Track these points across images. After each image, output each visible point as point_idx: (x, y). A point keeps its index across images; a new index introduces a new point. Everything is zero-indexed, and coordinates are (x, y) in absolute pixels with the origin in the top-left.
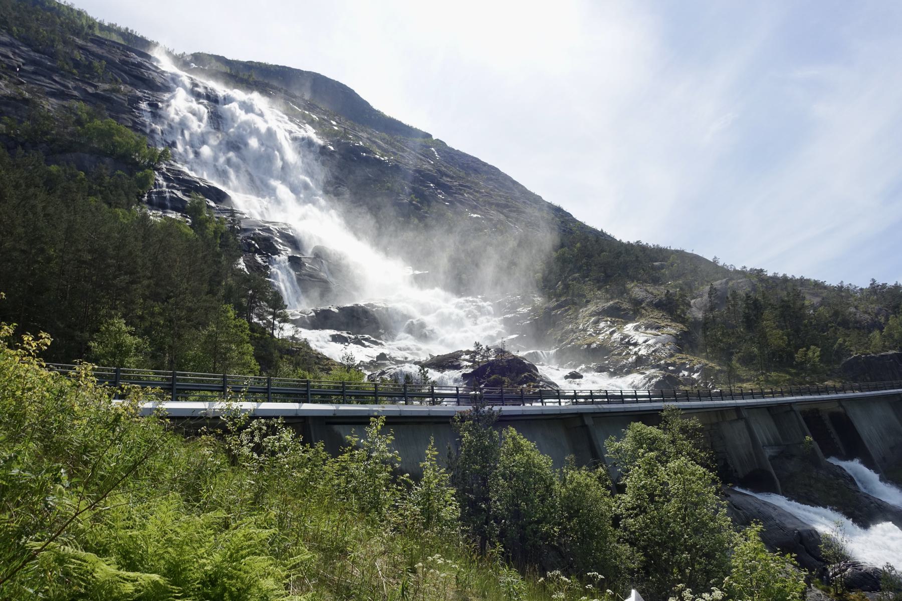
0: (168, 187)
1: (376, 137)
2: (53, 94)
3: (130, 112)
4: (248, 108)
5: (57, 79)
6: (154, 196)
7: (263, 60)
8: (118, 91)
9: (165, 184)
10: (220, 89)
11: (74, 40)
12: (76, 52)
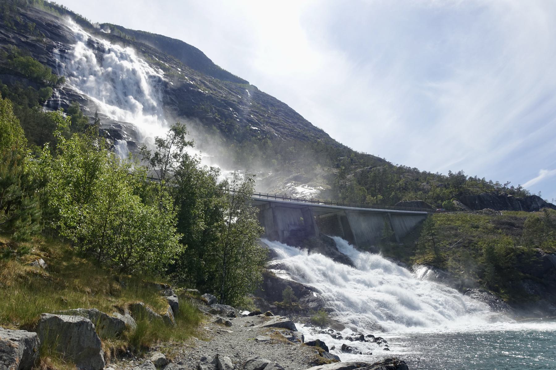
0: (61, 98)
1: (206, 80)
3: (47, 54)
5: (2, 32)
6: (51, 102)
7: (147, 30)
8: (41, 41)
9: (60, 96)
11: (18, 10)
12: (17, 17)
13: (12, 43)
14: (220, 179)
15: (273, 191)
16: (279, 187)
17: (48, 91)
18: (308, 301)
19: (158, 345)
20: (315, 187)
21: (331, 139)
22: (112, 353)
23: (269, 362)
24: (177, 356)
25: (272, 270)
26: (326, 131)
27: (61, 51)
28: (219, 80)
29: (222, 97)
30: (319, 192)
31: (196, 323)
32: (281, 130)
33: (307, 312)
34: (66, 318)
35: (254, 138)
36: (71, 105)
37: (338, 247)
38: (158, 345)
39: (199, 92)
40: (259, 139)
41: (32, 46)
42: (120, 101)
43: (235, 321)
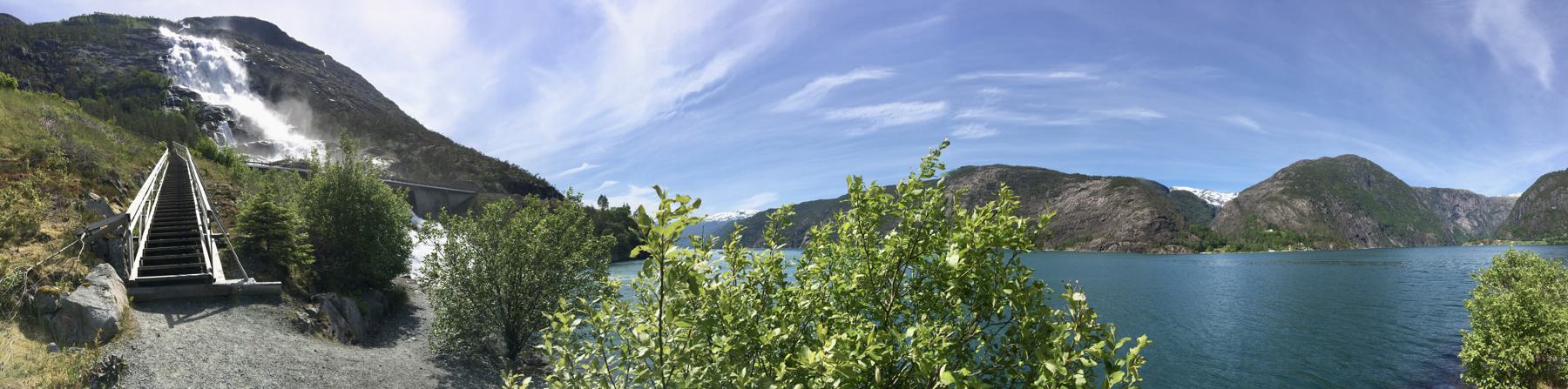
4: (210, 48)
10: (194, 40)
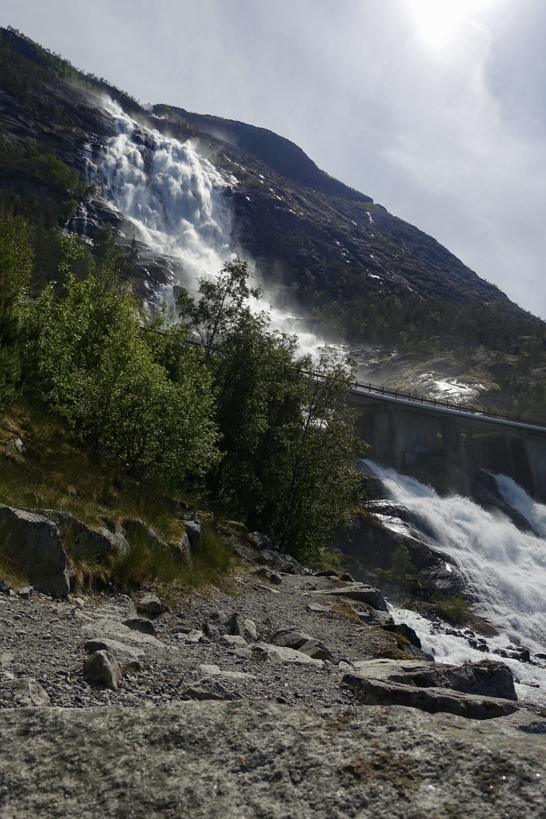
1: (302, 194)
2: (15, 131)
8: (69, 132)
9: (86, 213)
11: (44, 87)
12: (42, 97)
13: (32, 135)
14: (297, 356)
15: (395, 384)
16: (406, 378)
17: (71, 206)
18: (435, 577)
19: (154, 584)
20: (470, 383)
21: (511, 302)
22: (86, 579)
23: (310, 638)
24: (178, 605)
25: (378, 515)
26: (502, 287)
27: (93, 146)
28: (323, 195)
29: (325, 222)
30: (476, 392)
31: (224, 570)
32: (420, 282)
33: (431, 595)
34: (23, 515)
35: (372, 292)
36: (100, 227)
37: (502, 492)
38: (154, 584)
39: (288, 211)
40: (381, 296)
41: (56, 138)
42: (169, 225)
43: (289, 579)
